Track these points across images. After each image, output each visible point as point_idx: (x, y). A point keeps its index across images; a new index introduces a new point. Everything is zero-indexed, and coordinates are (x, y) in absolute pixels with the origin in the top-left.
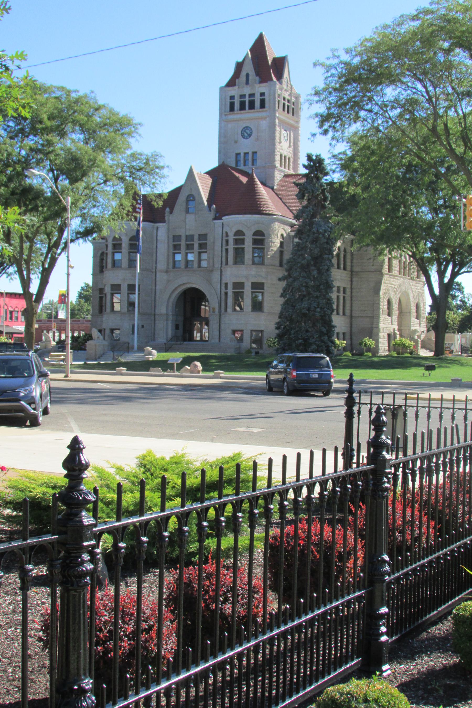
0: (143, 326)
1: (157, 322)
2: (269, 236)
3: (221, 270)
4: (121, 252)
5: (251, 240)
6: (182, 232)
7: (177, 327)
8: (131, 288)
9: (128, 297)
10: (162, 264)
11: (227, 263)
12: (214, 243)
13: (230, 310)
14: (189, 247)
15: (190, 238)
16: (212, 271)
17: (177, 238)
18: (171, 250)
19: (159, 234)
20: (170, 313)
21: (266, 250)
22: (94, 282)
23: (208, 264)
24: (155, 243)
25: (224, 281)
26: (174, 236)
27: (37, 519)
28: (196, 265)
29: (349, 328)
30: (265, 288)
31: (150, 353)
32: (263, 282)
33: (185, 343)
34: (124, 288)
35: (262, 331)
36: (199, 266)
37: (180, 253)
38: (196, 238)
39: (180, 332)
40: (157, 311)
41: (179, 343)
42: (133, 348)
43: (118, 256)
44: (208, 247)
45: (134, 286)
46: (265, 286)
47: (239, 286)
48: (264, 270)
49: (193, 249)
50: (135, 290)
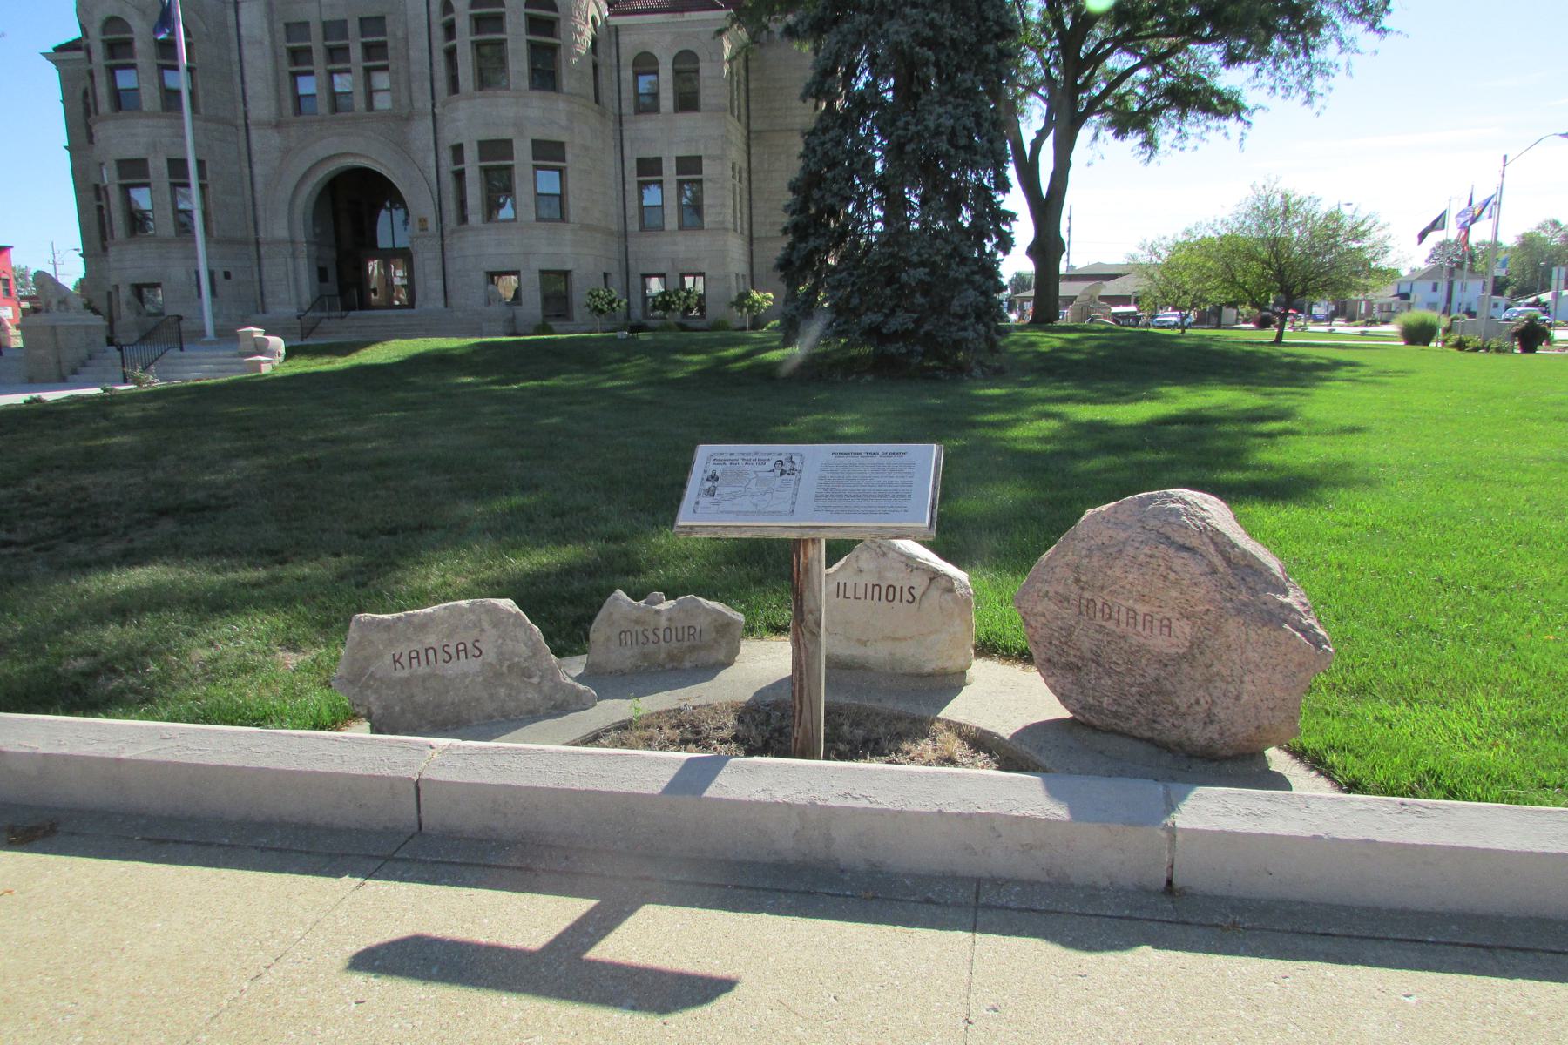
0: (227, 275)
1: (265, 262)
2: (570, 16)
3: (434, 115)
4: (133, 66)
5: (523, 20)
6: (311, 13)
7: (322, 275)
8: (177, 167)
9: (175, 203)
10: (262, 105)
11: (454, 86)
12: (406, 40)
13: (475, 218)
14: (337, 54)
15: (334, 28)
16: (408, 119)
17: (296, 29)
18: (286, 66)
19: (244, 19)
20: (301, 237)
21: (563, 51)
22: (593, 964)
23: (395, 101)
24: (235, 45)
25: (449, 137)
26: (287, 25)
27: (77, 689)
28: (359, 103)
29: (748, 265)
30: (568, 157)
31: (261, 348)
32: (562, 139)
33: (352, 313)
34: (158, 167)
35: (566, 274)
36: (370, 106)
37: (311, 73)
38: (353, 27)
39: (332, 286)
40: (262, 234)
41: (334, 314)
42: (202, 333)
43: (125, 80)
44: (390, 53)
45: (184, 162)
46: (568, 149)
47: (496, 149)
48: (562, 105)
49: (348, 60)
50: (186, 176)
